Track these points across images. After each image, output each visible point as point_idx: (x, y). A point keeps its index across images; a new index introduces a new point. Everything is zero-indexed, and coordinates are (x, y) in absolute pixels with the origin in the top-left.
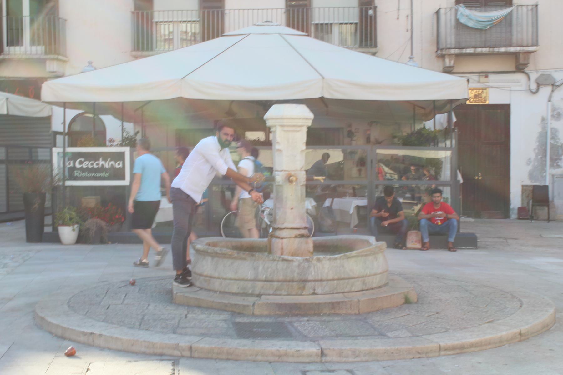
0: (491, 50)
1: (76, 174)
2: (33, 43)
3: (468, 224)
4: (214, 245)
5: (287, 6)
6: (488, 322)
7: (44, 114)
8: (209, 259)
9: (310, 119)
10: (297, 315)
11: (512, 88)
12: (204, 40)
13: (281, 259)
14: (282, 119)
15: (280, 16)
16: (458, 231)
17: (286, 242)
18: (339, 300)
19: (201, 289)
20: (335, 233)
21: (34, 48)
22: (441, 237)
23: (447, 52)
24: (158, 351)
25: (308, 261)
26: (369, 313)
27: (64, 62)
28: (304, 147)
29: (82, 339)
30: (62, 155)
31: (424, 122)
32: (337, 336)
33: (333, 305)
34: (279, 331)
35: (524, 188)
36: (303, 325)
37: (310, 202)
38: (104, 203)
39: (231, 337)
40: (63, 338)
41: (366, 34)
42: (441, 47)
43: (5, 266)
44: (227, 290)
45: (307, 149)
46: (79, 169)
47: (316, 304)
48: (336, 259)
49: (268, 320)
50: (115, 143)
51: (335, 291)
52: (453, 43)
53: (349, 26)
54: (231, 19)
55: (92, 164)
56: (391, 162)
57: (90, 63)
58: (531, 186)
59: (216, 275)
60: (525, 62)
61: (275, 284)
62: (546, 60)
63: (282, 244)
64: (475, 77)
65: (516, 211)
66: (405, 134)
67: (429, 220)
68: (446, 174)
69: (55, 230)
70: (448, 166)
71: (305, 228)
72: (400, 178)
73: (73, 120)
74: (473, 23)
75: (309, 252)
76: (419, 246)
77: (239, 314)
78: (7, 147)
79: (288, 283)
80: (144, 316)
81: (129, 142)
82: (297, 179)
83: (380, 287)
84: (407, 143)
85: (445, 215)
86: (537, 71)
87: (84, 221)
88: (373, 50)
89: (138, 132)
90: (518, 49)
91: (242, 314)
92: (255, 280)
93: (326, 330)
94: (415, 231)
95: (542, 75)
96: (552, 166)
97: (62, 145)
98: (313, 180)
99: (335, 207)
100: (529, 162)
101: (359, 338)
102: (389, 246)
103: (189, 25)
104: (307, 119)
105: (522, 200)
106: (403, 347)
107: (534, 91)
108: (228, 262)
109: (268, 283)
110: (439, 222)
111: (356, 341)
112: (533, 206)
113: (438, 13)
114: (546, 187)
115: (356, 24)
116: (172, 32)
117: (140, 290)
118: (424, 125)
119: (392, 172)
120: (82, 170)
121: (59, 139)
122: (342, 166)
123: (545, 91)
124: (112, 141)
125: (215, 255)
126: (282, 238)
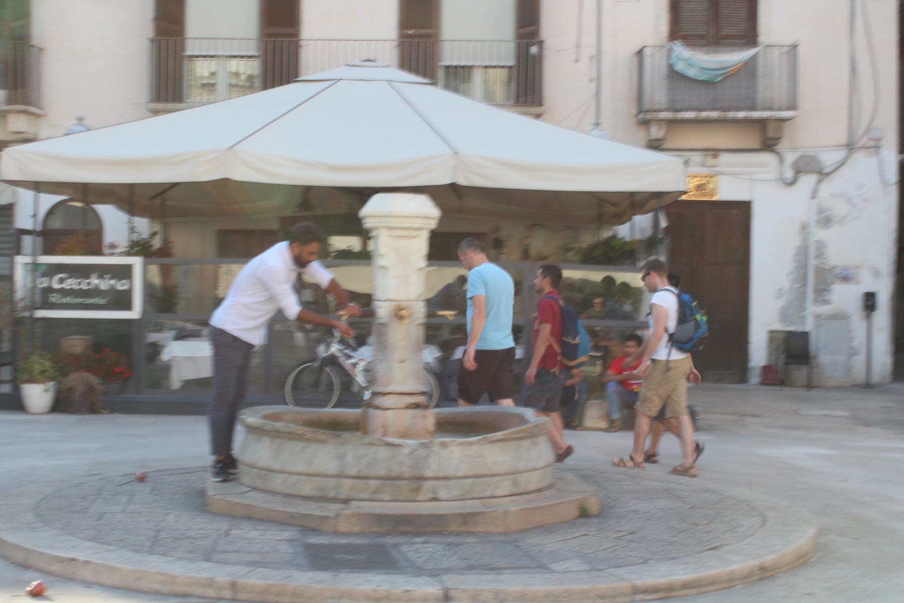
1: (54, 298)
4: (275, 417)
15: (389, 52)
17: (392, 415)
19: (254, 489)
24: (180, 589)
25: (424, 446)
27: (38, 116)
28: (423, 263)
29: (56, 568)
30: (30, 268)
33: (466, 518)
34: (378, 559)
36: (417, 549)
38: (97, 347)
39: (298, 567)
40: (24, 566)
41: (526, 86)
45: (429, 265)
48: (470, 444)
50: (118, 251)
54: (310, 55)
57: (81, 119)
59: (277, 466)
60: (776, 136)
64: (697, 157)
66: (584, 245)
69: (17, 390)
71: (423, 393)
73: (51, 212)
76: (603, 424)
80: (160, 531)
81: (140, 248)
86: (794, 149)
87: (65, 375)
88: (537, 110)
90: (765, 114)
92: (340, 476)
95: (802, 157)
96: (816, 301)
100: (780, 294)
108: (297, 446)
111: (501, 577)
113: (640, 53)
114: (805, 335)
115: (510, 67)
120: (64, 292)
123: (808, 181)
124: (112, 246)
125: (275, 435)
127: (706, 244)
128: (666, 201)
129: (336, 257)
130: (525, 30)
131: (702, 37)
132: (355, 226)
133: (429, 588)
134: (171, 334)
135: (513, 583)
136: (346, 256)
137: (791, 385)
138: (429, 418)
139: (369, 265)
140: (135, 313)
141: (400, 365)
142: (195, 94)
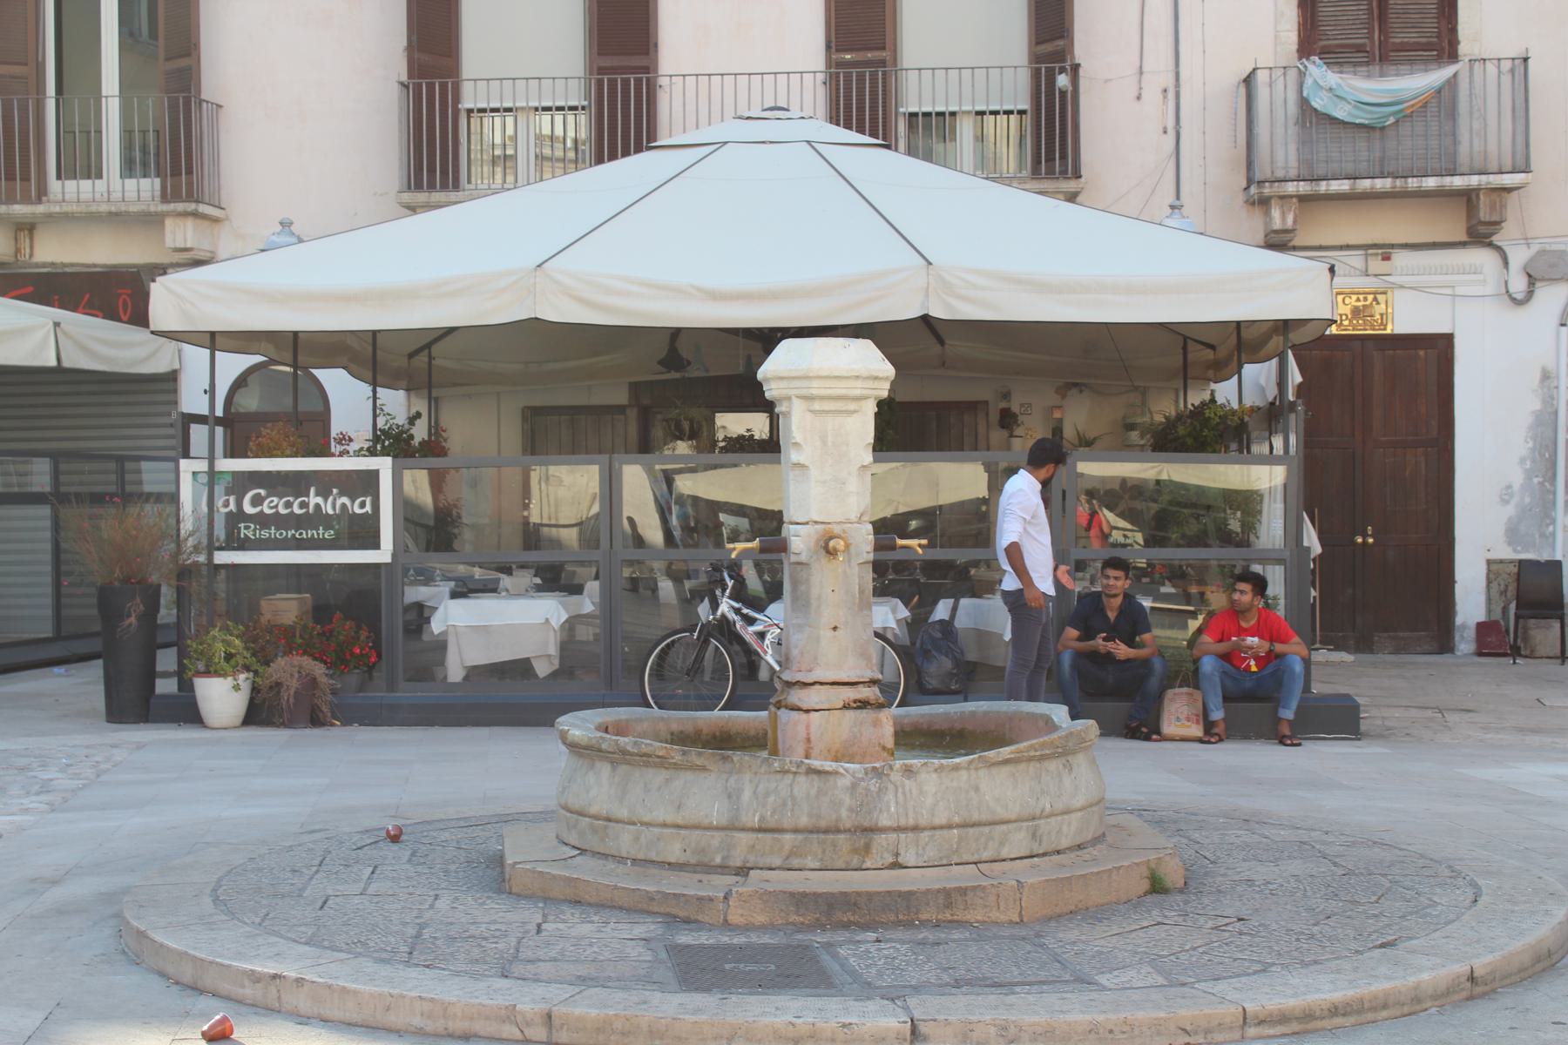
0: (1399, 182)
1: (247, 531)
2: (129, 167)
3: (1334, 671)
4: (620, 729)
5: (829, 63)
6: (1383, 946)
7: (160, 366)
8: (605, 769)
9: (887, 378)
10: (846, 926)
11: (1459, 290)
12: (600, 160)
13: (803, 769)
14: (807, 378)
15: (812, 94)
16: (1307, 688)
17: (818, 723)
18: (963, 885)
19: (583, 851)
20: (964, 694)
21: (131, 184)
22: (1258, 706)
23: (1278, 189)
24: (459, 1026)
26: (1050, 919)
27: (216, 220)
28: (868, 457)
29: (248, 991)
30: (204, 479)
31: (1213, 386)
32: (957, 984)
33: (949, 897)
34: (796, 971)
35: (1494, 567)
36: (862, 952)
37: (894, 611)
38: (321, 612)
39: (661, 986)
40: (197, 989)
41: (1051, 144)
42: (1258, 176)
43: (45, 788)
44: (653, 856)
45: (876, 460)
46: (250, 518)
47: (900, 894)
48: (956, 768)
49: (766, 939)
50: (354, 447)
51: (956, 859)
52: (1293, 163)
53: (1002, 119)
54: (671, 104)
55: (288, 505)
56: (1121, 496)
57: (286, 224)
58: (1511, 562)
59: (623, 813)
60: (1495, 218)
61: (788, 837)
62: (1552, 212)
63: (808, 727)
64: (1356, 259)
65: (1471, 633)
66: (1159, 418)
67: (1226, 657)
68: (1272, 529)
69: (187, 687)
70: (1279, 507)
71: (873, 682)
72: (1151, 542)
73: (240, 383)
74: (1348, 107)
75: (884, 748)
76: (1197, 731)
77: (687, 921)
78: (56, 457)
79: (822, 836)
80: (422, 926)
81: (392, 442)
82: (847, 546)
83: (1080, 847)
84: (1175, 439)
85: (1266, 645)
86: (1527, 241)
87: (267, 663)
88: (1071, 185)
89: (418, 415)
90: (1474, 180)
91: (696, 921)
93: (926, 968)
94: (1185, 690)
95: (1542, 253)
97: (206, 454)
98: (893, 547)
99: (961, 622)
100: (1505, 496)
101: (1018, 989)
102: (1107, 731)
103: (559, 118)
104: (876, 378)
105: (1489, 600)
106: (1140, 1015)
107: (1519, 296)
108: (657, 777)
109: (769, 836)
110: (1253, 663)
111: (1011, 999)
112: (1517, 617)
113: (1249, 81)
114: (1557, 565)
115: (1021, 112)
116: (515, 138)
117: (413, 854)
118: (1213, 392)
119: (1129, 526)
120: (262, 520)
121: (198, 433)
122: (984, 508)
124: (344, 439)
125: (619, 758)
126: (808, 711)
127: (1375, 413)
128: (1297, 337)
129: (724, 450)
130: (1048, 48)
131: (1359, 49)
132: (752, 397)
133: (887, 1020)
134: (446, 588)
135: (1031, 1010)
136: (744, 446)
137: (1531, 656)
138: (886, 723)
139: (776, 466)
140: (383, 555)
141: (832, 631)
142: (481, 174)
